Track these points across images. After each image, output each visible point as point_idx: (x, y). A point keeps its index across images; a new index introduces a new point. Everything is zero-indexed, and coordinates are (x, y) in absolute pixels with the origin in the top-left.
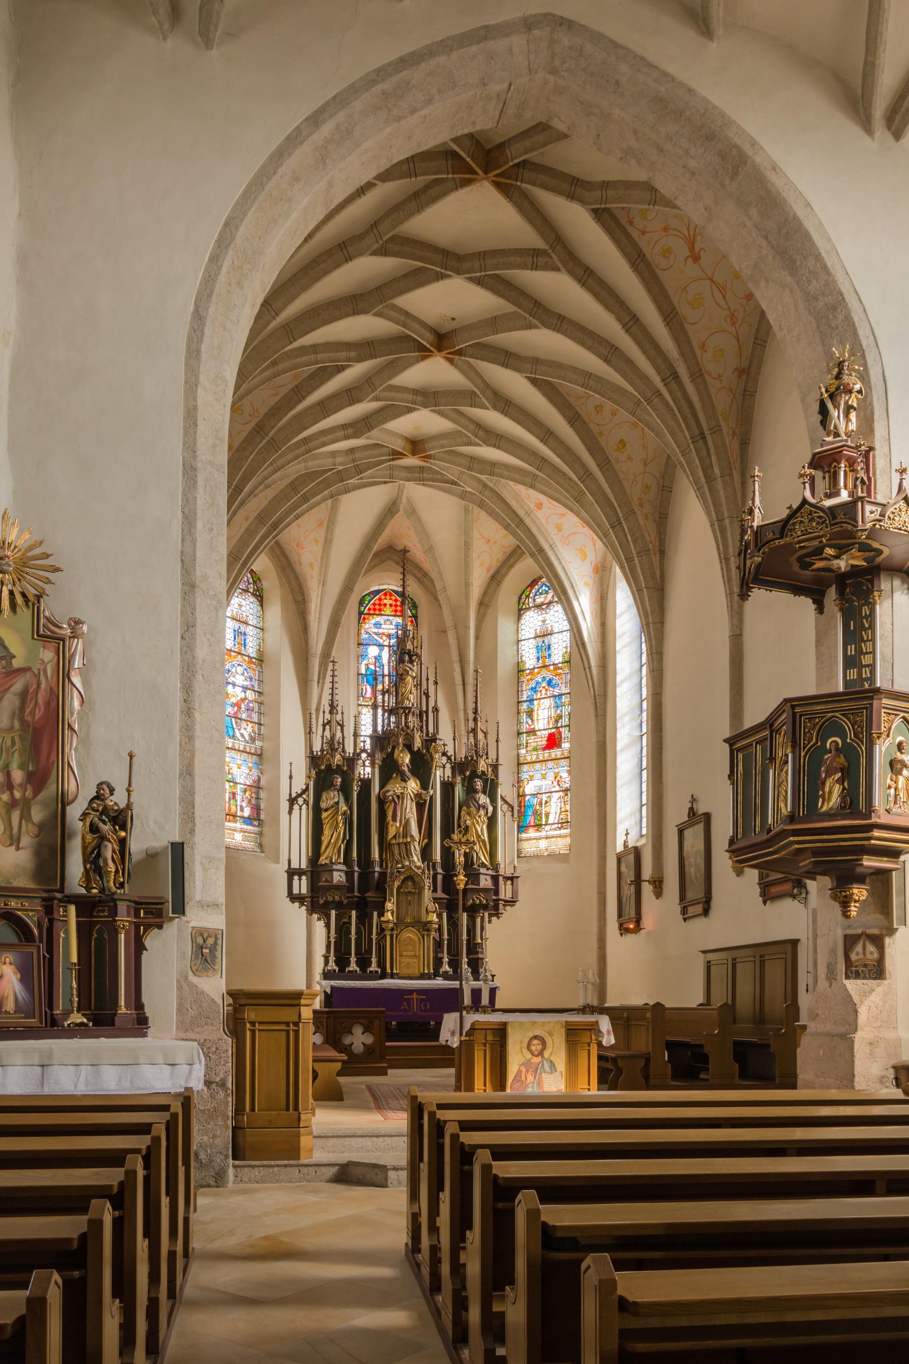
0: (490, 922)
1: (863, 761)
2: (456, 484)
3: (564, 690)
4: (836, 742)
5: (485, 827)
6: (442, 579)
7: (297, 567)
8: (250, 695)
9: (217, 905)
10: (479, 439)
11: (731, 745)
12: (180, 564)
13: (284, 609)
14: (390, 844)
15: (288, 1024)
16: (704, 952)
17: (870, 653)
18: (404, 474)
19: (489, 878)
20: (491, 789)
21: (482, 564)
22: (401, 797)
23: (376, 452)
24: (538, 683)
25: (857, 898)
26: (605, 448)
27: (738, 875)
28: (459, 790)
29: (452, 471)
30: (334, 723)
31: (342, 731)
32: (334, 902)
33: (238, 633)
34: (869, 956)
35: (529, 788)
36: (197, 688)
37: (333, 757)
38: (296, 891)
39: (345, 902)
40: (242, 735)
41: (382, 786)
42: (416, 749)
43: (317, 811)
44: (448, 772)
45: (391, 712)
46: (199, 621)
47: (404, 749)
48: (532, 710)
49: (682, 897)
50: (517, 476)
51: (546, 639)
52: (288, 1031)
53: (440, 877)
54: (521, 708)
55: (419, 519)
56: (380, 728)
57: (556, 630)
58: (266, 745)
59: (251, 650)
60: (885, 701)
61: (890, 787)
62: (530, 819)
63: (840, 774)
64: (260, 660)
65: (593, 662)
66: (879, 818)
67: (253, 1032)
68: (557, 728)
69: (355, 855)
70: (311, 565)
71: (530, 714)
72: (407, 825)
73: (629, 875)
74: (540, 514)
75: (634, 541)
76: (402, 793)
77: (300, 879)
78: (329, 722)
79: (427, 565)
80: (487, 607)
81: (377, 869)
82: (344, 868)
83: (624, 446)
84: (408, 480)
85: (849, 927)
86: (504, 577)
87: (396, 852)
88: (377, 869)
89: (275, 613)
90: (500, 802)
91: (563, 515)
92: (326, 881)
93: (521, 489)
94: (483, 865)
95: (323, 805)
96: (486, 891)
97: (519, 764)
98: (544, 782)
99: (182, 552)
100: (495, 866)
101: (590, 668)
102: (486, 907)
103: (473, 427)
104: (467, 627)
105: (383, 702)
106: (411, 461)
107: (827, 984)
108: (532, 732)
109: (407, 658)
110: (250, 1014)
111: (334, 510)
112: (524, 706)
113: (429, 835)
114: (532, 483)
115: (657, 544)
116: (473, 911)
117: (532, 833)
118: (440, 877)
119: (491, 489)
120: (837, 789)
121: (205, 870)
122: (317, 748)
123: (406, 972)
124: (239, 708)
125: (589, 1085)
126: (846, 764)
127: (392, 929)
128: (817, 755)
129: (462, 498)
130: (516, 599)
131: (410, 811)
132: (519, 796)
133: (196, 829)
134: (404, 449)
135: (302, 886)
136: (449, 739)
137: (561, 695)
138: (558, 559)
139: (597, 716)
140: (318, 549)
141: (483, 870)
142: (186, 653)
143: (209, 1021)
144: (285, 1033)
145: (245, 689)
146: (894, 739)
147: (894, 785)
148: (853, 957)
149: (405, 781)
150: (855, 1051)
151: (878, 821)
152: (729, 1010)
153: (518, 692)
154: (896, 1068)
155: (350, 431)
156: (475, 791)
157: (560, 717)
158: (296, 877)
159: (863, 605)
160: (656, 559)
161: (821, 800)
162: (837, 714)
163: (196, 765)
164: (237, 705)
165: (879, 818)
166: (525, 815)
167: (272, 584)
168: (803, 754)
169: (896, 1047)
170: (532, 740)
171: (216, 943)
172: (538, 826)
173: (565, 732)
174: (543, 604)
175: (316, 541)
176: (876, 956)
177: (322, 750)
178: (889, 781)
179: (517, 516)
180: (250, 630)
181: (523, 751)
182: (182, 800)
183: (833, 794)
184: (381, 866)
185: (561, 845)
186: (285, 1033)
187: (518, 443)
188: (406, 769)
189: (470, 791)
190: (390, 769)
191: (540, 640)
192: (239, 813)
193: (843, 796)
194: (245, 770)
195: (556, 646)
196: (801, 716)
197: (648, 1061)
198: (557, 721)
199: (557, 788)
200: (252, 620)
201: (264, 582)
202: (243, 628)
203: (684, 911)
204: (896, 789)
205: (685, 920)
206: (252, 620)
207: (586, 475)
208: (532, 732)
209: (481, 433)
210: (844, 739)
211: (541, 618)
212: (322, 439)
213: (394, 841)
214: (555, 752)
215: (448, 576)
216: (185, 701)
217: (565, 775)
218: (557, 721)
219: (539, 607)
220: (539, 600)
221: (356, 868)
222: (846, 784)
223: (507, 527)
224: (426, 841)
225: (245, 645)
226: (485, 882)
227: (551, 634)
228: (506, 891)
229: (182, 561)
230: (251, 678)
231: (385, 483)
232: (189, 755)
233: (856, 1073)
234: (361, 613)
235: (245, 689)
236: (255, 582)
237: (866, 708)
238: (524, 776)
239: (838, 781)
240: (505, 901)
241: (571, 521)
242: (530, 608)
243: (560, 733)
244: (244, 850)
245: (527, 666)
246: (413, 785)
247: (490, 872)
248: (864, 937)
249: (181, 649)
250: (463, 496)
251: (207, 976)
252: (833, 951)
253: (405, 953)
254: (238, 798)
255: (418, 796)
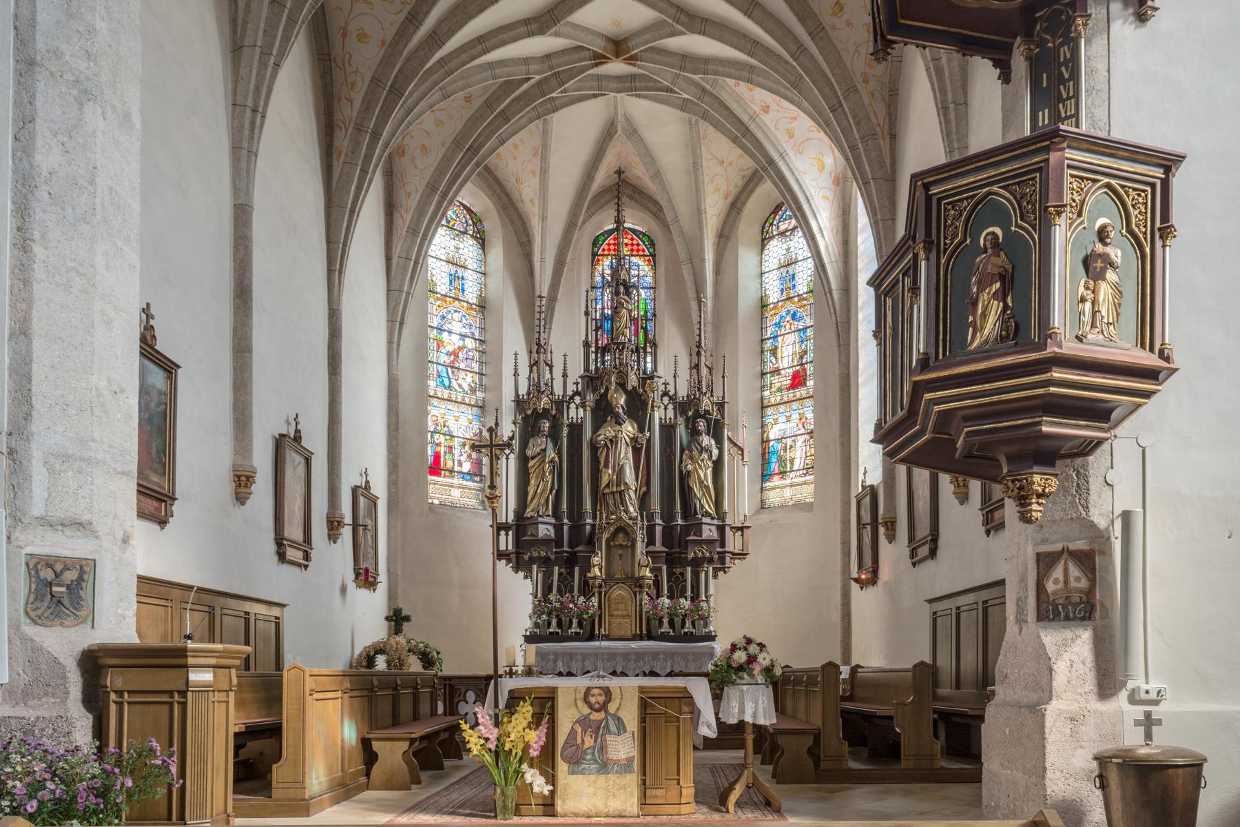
0: (715, 577)
1: (1035, 257)
2: (671, 91)
3: (809, 322)
4: (993, 233)
5: (709, 471)
6: (673, 208)
7: (519, 205)
8: (470, 343)
9: (80, 524)
10: (682, 25)
11: (877, 288)
12: (12, 32)
13: (507, 251)
14: (604, 494)
15: (171, 693)
16: (930, 601)
17: (1071, 116)
18: (615, 85)
19: (714, 528)
20: (716, 431)
21: (717, 190)
22: (614, 441)
23: (575, 56)
24: (782, 317)
25: (1040, 490)
26: (818, 12)
27: (962, 503)
28: (681, 432)
29: (664, 74)
30: (542, 363)
31: (551, 372)
32: (539, 558)
33: (454, 278)
34: (1073, 584)
35: (773, 433)
36: (37, 211)
37: (539, 399)
38: (502, 547)
39: (553, 557)
40: (460, 386)
41: (596, 429)
42: (630, 388)
43: (523, 460)
44: (670, 413)
45: (604, 350)
46: (41, 113)
47: (613, 384)
48: (776, 348)
49: (911, 539)
50: (732, 71)
51: (790, 269)
52: (171, 704)
53: (658, 530)
54: (764, 347)
55: (641, 140)
56: (592, 367)
57: (800, 258)
58: (489, 396)
59: (470, 296)
60: (1069, 153)
61: (1083, 300)
62: (774, 467)
63: (998, 285)
64: (483, 306)
65: (834, 286)
66: (1060, 347)
67: (120, 705)
68: (802, 365)
69: (565, 507)
70: (532, 200)
71: (774, 352)
72: (620, 472)
73: (867, 518)
74: (767, 119)
75: (857, 124)
76: (616, 437)
77: (507, 535)
78: (536, 363)
79: (651, 187)
80: (728, 238)
81: (589, 521)
82: (553, 521)
83: (842, 9)
84: (619, 91)
85: (1044, 541)
86: (744, 204)
87: (611, 502)
88: (589, 521)
89: (497, 254)
90: (726, 443)
91: (795, 118)
92: (532, 535)
93: (743, 88)
94: (707, 514)
95: (529, 453)
96: (710, 542)
97: (763, 408)
98: (789, 425)
99: (16, 16)
100: (720, 515)
101: (831, 292)
102: (710, 561)
103: (673, 11)
104: (703, 260)
105: (597, 340)
106: (616, 67)
107: (1016, 629)
108: (777, 371)
109: (622, 289)
110: (112, 680)
111: (545, 133)
112: (768, 344)
113: (648, 483)
114: (745, 73)
115: (886, 127)
116: (697, 564)
117: (776, 481)
118: (658, 530)
119: (711, 94)
120: (996, 308)
121: (51, 471)
122: (523, 390)
123: (617, 633)
124: (457, 356)
125: (678, 774)
126: (1009, 267)
127: (600, 586)
128: (963, 254)
129: (683, 109)
130: (758, 228)
131: (625, 456)
132: (763, 442)
133: (34, 413)
134: (605, 49)
135: (507, 542)
136: (670, 366)
137: (806, 328)
138: (790, 170)
139: (839, 346)
140: (535, 181)
141: (705, 520)
142: (21, 160)
143: (50, 690)
144: (166, 708)
145: (463, 336)
146: (1092, 221)
147: (1090, 296)
148: (1050, 587)
149: (620, 424)
150: (1047, 731)
151: (1057, 350)
152: (926, 673)
153: (762, 329)
154: (1102, 760)
155: (534, 26)
156: (698, 433)
157: (805, 352)
158: (503, 533)
159: (1062, 45)
160: (885, 145)
161: (971, 330)
162: (995, 188)
163: (34, 321)
164: (455, 354)
165: (1060, 347)
166: (768, 464)
167: (493, 224)
168: (943, 261)
169: (1114, 725)
170: (775, 379)
171: (81, 579)
172: (783, 473)
173: (810, 369)
174: (787, 231)
175: (533, 173)
176: (1084, 584)
177: (528, 394)
178: (1081, 289)
179: (742, 123)
180: (469, 275)
181: (767, 393)
182: (13, 371)
183: (990, 319)
184: (594, 518)
185: (806, 493)
186: (166, 708)
187: (726, 27)
188: (621, 411)
189: (694, 433)
190: (603, 412)
191: (784, 270)
192: (456, 468)
193: (1004, 319)
194: (464, 421)
195: (800, 275)
196: (939, 201)
197: (817, 737)
198: (801, 357)
199: (803, 431)
200: (472, 264)
201: (485, 224)
202: (460, 272)
203: (913, 553)
204: (1093, 303)
205: (914, 564)
206: (472, 264)
207: (799, 50)
208: (777, 371)
209: (683, 18)
210: (1006, 230)
211: (785, 246)
212: (501, 37)
213: (607, 491)
214: (801, 392)
215: (683, 207)
216: (19, 229)
217: (810, 415)
218: (801, 357)
219: (782, 234)
220: (783, 227)
221: (566, 521)
222: (1009, 300)
223: (734, 140)
224: (644, 489)
225: (463, 290)
226: (709, 532)
227: (795, 263)
228: (733, 543)
229: (16, 28)
230: (470, 325)
231: (595, 96)
232: (24, 306)
233: (1048, 765)
234: (594, 255)
235: (463, 336)
236: (474, 224)
237: (1040, 170)
238: (769, 420)
239: (995, 296)
240: (733, 554)
241: (804, 124)
242: (773, 237)
243: (805, 370)
244: (463, 508)
245: (771, 300)
246: (630, 428)
247: (715, 522)
248: (1065, 555)
249: (14, 155)
250: (684, 106)
251: (61, 624)
252: (1023, 580)
253: (616, 613)
254: (456, 452)
255: (634, 440)
